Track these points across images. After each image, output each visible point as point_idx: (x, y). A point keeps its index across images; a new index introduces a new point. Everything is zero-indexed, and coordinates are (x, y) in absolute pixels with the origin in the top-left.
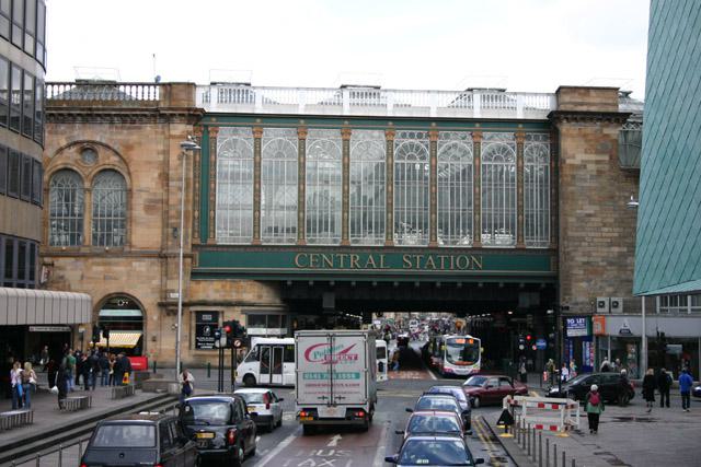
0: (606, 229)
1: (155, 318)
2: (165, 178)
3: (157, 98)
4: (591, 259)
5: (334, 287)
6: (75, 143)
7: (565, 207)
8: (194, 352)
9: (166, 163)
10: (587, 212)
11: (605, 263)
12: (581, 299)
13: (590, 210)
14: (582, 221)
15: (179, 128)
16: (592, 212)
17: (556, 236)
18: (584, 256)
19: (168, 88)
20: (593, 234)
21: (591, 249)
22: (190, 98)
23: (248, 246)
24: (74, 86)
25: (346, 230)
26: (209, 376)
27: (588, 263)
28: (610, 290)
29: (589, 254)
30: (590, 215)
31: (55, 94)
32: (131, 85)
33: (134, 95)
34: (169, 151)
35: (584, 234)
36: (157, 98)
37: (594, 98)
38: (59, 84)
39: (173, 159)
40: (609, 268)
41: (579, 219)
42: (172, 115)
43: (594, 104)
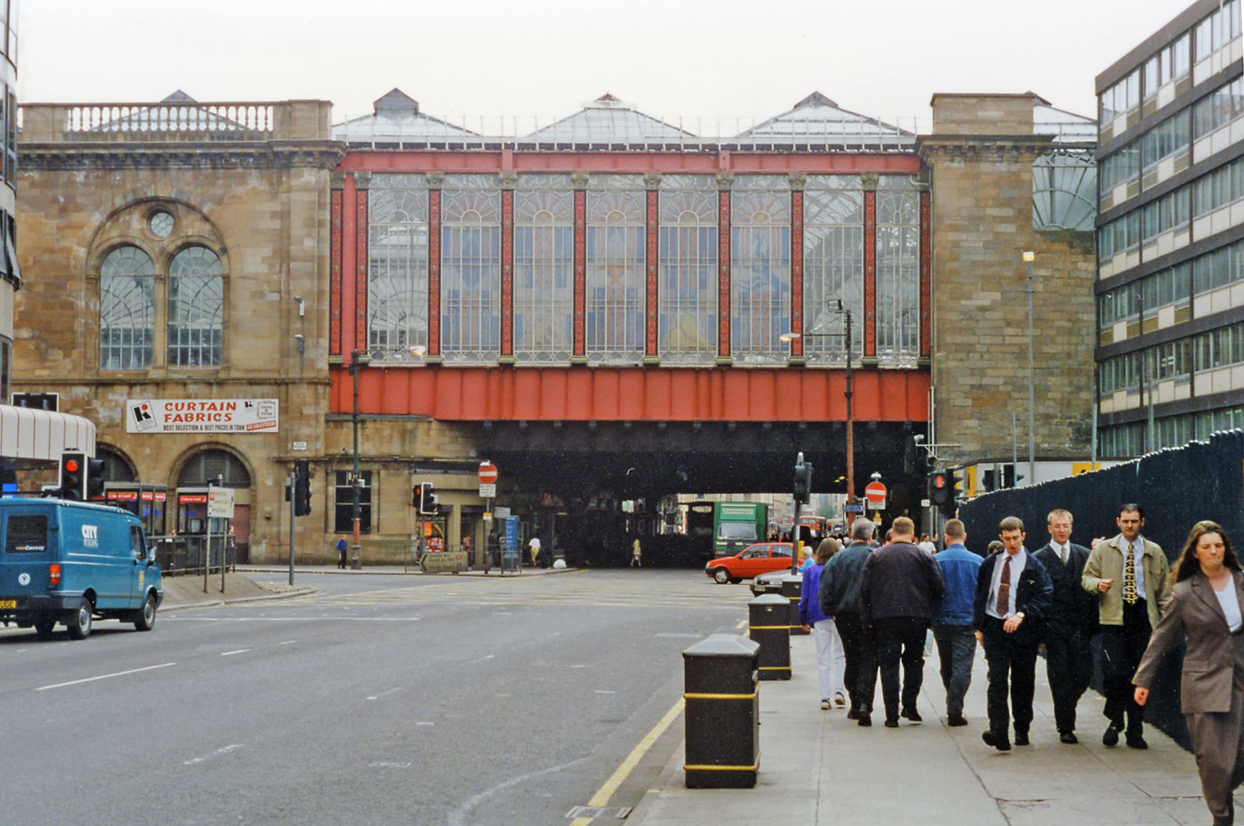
0: (1010, 331)
1: (269, 482)
2: (283, 256)
3: (270, 128)
4: (985, 381)
5: (700, 431)
6: (138, 202)
7: (939, 296)
8: (332, 537)
9: (284, 236)
10: (980, 303)
11: (1009, 388)
12: (326, 549)
13: (985, 298)
14: (970, 318)
15: (310, 177)
16: (986, 302)
17: (926, 351)
18: (972, 375)
19: (285, 108)
20: (988, 340)
21: (986, 364)
22: (323, 122)
23: (492, 369)
24: (890, 357)
25: (579, 338)
26: (291, 583)
27: (980, 387)
28: (135, 553)
29: (982, 372)
30: (982, 309)
31: (96, 123)
32: (237, 105)
33: (242, 121)
34: (289, 213)
35: (972, 339)
36: (270, 128)
37: (991, 112)
38: (111, 106)
39: (297, 229)
40: (1016, 395)
41: (968, 315)
42: (293, 154)
43: (993, 120)
